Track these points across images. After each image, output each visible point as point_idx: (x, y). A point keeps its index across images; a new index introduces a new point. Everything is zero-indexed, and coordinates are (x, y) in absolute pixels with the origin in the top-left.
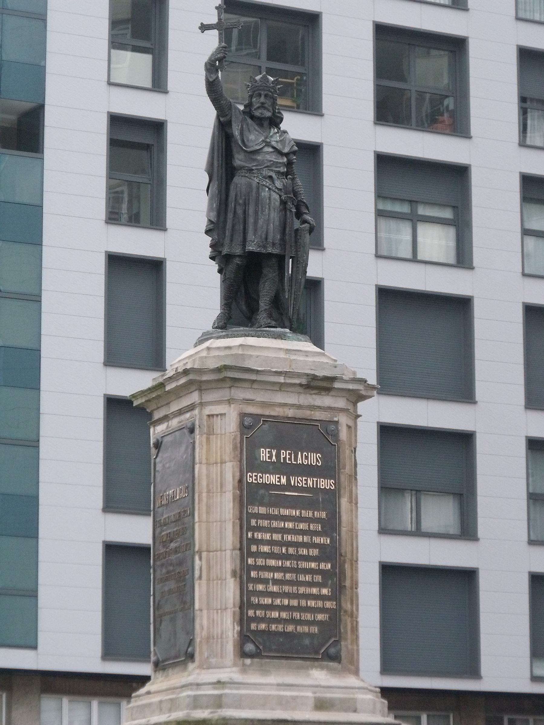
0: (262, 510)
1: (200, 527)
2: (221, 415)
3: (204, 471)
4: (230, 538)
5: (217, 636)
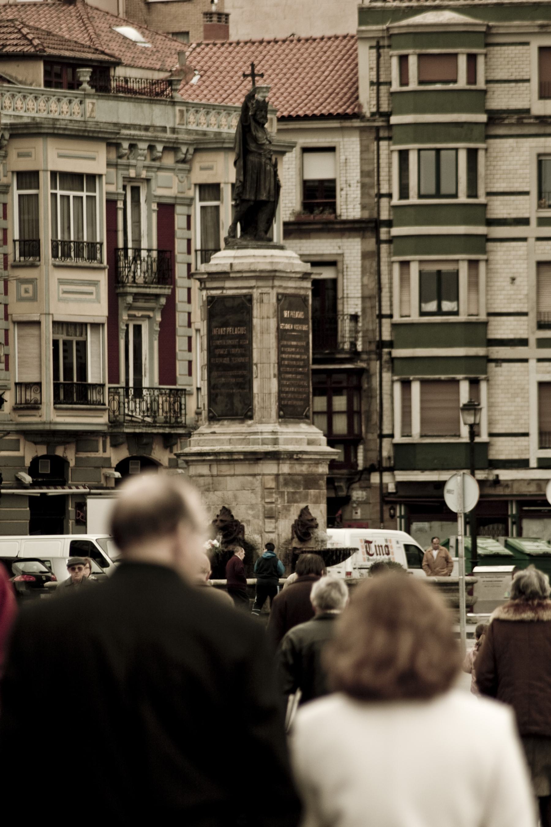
4: (273, 357)
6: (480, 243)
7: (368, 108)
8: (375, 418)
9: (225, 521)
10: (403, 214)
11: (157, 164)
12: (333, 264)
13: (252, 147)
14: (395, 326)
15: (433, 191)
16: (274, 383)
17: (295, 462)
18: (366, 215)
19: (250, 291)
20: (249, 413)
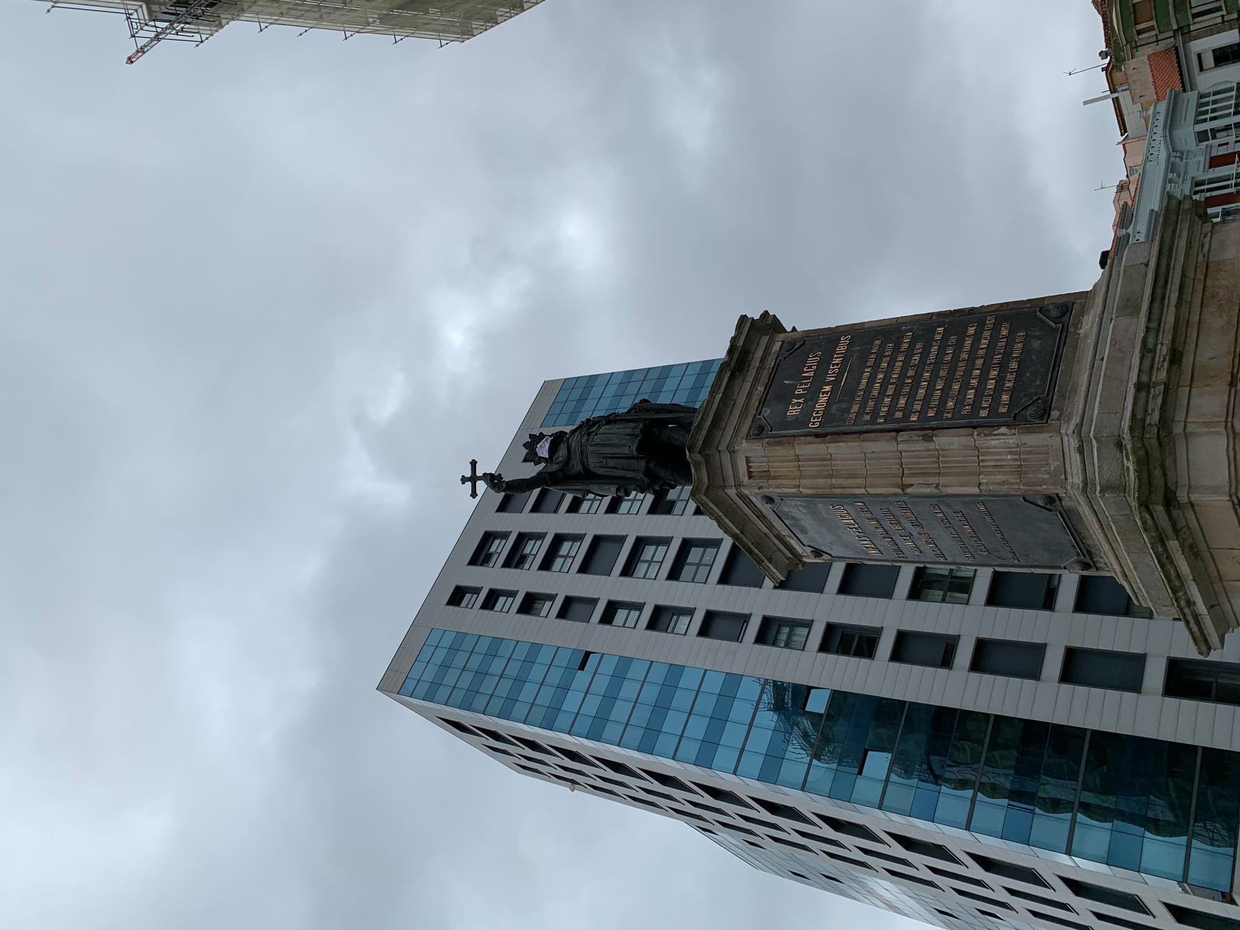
1: (871, 486)
4: (881, 446)
5: (1016, 460)
17: (1188, 361)
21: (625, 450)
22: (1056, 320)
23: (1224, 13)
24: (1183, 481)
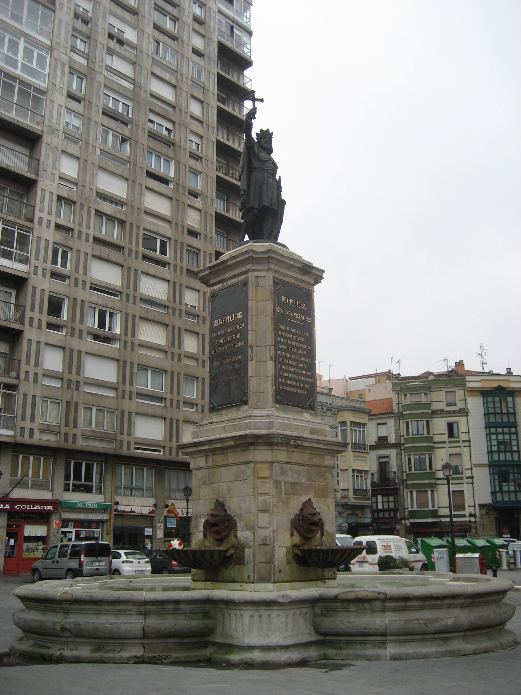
0: (284, 327)
2: (263, 276)
3: (254, 305)
4: (270, 339)
6: (432, 448)
7: (396, 409)
8: (402, 503)
9: (217, 516)
10: (407, 440)
11: (325, 414)
12: (388, 457)
13: (256, 164)
14: (407, 474)
15: (417, 433)
16: (271, 365)
17: (295, 450)
18: (397, 442)
19: (245, 276)
20: (244, 398)
21: (265, 198)
22: (310, 405)
23: (406, 437)
24: (256, 448)
